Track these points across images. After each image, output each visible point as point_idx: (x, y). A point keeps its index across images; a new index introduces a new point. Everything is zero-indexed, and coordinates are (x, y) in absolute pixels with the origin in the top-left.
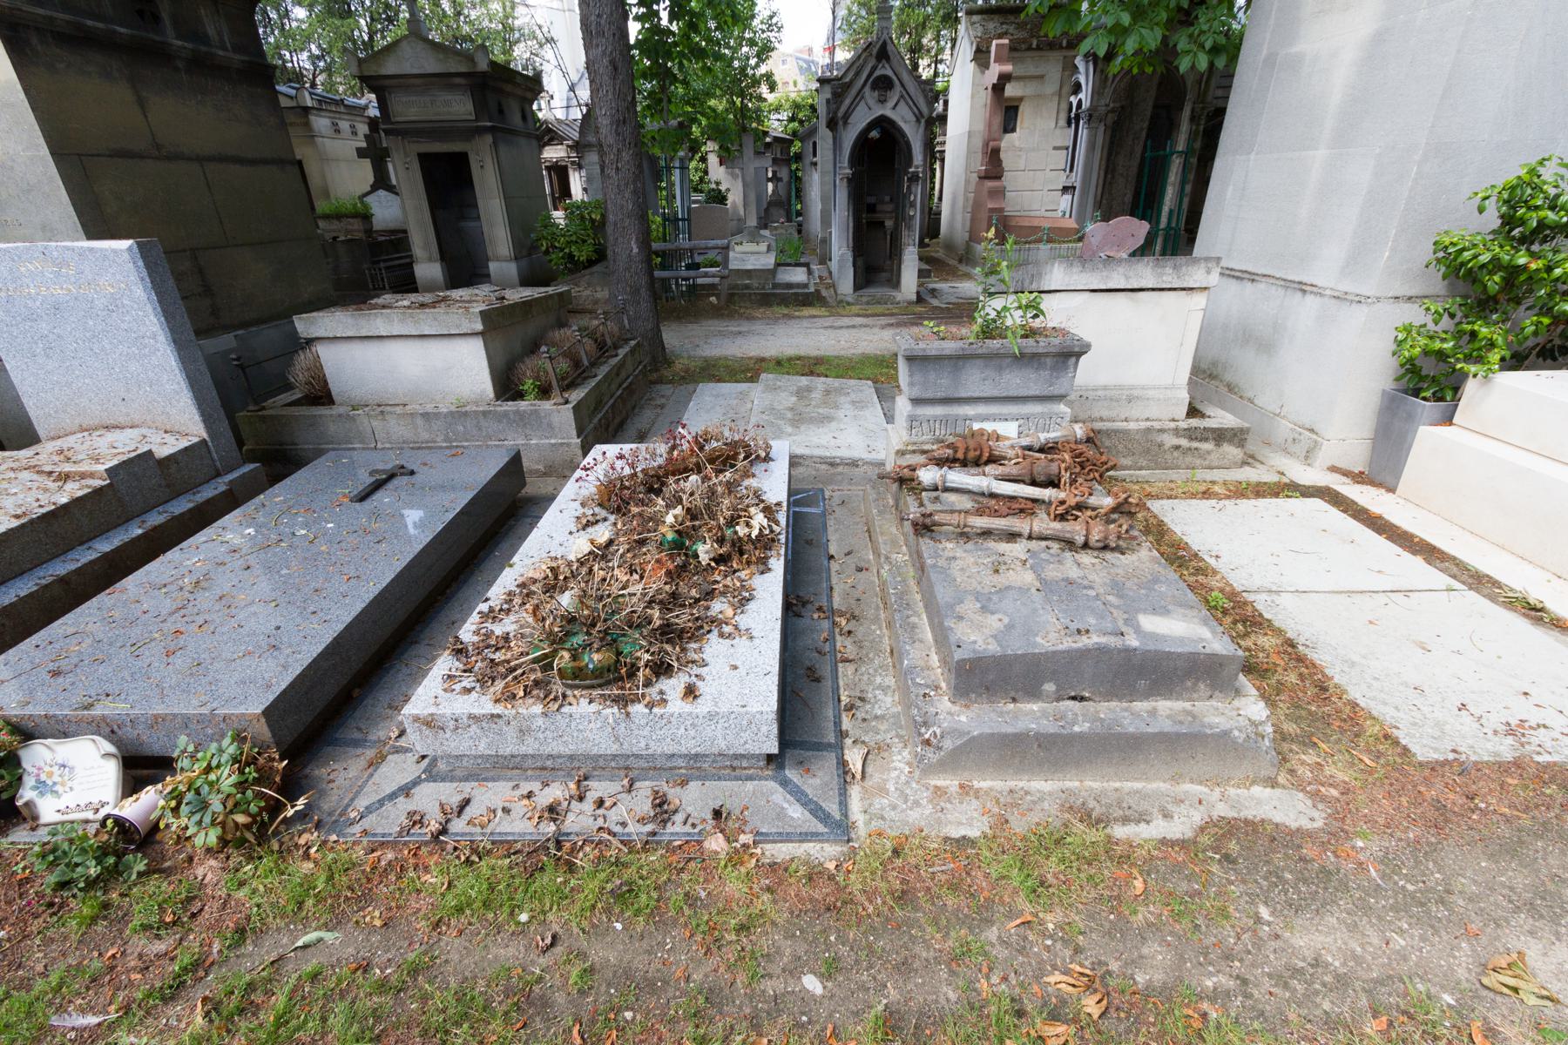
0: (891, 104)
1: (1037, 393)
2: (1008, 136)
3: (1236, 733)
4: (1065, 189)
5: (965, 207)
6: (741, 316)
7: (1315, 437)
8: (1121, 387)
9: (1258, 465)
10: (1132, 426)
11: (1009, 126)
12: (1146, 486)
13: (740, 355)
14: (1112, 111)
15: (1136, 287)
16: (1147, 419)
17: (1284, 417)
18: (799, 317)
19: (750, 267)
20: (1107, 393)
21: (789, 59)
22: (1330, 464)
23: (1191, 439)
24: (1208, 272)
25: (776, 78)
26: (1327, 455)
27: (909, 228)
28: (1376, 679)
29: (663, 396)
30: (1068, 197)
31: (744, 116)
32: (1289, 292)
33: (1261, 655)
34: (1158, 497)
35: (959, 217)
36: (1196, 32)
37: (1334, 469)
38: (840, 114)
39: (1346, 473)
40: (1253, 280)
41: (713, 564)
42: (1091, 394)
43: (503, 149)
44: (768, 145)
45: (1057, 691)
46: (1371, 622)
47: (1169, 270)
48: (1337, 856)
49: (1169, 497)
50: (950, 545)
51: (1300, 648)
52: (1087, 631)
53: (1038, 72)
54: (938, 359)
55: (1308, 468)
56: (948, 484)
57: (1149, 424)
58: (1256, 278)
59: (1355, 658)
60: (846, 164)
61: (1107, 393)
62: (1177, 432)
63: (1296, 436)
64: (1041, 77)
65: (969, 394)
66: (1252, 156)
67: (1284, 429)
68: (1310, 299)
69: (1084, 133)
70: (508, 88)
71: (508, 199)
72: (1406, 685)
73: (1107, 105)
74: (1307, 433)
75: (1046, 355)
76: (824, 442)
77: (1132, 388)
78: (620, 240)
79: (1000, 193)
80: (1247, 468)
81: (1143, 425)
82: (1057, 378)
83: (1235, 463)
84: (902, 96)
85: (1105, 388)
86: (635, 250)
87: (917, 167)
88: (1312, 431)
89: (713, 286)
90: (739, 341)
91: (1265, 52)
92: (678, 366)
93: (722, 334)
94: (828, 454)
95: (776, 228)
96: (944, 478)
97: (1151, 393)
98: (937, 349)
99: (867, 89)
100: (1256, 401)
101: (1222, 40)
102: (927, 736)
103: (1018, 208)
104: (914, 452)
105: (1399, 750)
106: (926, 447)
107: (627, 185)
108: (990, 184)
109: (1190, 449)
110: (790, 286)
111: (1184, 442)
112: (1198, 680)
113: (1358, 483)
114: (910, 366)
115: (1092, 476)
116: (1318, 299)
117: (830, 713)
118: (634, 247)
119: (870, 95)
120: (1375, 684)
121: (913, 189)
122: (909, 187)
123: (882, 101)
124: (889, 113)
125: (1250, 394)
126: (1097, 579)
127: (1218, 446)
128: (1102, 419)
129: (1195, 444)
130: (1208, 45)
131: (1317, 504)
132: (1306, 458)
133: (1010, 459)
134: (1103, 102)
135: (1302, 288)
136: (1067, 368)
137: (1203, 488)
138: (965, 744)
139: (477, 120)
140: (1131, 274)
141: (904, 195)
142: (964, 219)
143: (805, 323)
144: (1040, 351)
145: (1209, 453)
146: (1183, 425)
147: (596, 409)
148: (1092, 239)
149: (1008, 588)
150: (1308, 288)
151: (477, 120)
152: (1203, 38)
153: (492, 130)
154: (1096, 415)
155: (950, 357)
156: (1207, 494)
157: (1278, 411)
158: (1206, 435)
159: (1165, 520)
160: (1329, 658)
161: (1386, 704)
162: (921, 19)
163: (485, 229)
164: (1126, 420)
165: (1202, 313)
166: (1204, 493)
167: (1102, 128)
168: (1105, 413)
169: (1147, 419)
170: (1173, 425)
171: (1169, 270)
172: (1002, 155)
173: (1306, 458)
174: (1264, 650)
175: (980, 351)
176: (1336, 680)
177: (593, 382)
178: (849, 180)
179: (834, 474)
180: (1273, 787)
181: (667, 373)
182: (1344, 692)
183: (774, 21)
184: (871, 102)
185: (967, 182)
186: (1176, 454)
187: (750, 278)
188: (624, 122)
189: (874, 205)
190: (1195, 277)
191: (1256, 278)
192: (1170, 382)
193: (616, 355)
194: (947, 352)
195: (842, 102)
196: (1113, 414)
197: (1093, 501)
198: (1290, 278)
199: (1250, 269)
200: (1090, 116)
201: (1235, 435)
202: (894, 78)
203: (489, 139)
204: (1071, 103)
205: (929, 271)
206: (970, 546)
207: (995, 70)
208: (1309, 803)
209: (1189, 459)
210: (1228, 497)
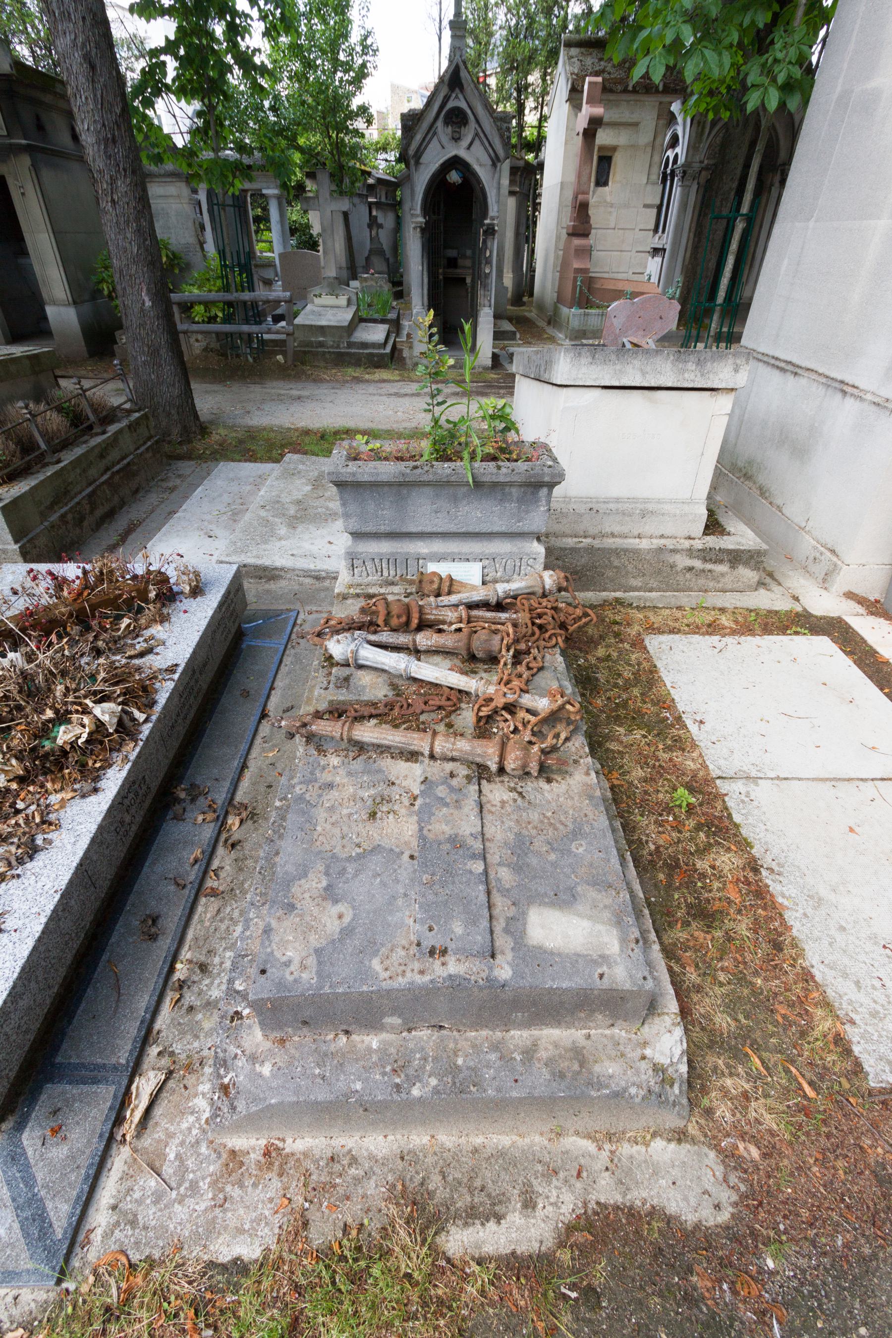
0: (465, 143)
1: (503, 529)
2: (601, 189)
3: (633, 1090)
4: (656, 251)
5: (555, 266)
6: (308, 377)
7: (835, 559)
8: (635, 500)
9: (775, 588)
10: (644, 544)
11: (602, 180)
12: (650, 614)
13: (288, 425)
14: (706, 168)
15: (653, 384)
16: (662, 536)
17: (808, 532)
18: (367, 381)
19: (323, 323)
20: (620, 506)
21: (414, 96)
22: (846, 589)
23: (705, 560)
24: (736, 370)
25: (373, 111)
26: (845, 580)
27: (485, 286)
28: (842, 929)
29: (179, 476)
30: (658, 259)
31: (340, 153)
32: (830, 391)
33: (716, 885)
34: (660, 631)
35: (550, 276)
36: (770, 61)
37: (850, 595)
38: (411, 151)
39: (861, 601)
40: (796, 374)
41: (14, 786)
42: (602, 507)
43: (47, 174)
44: (371, 187)
45: (404, 1023)
46: (851, 830)
47: (691, 366)
48: (735, 1293)
49: (672, 631)
50: (334, 760)
51: (764, 873)
52: (444, 952)
53: (634, 118)
54: (375, 486)
55: (823, 592)
56: (361, 662)
57: (663, 541)
58: (799, 371)
59: (824, 892)
60: (418, 211)
61: (620, 506)
62: (690, 552)
63: (818, 555)
64: (636, 124)
65: (419, 529)
66: (811, 224)
67: (806, 545)
68: (849, 402)
69: (677, 191)
70: (48, 98)
71: (58, 234)
72: (873, 938)
73: (701, 162)
74: (828, 554)
75: (511, 484)
76: (314, 549)
77: (646, 501)
78: (129, 290)
79: (586, 252)
80: (762, 591)
81: (657, 543)
82: (527, 512)
83: (750, 587)
84: (477, 135)
85: (617, 500)
86: (148, 304)
87: (493, 219)
88: (833, 551)
89: (283, 343)
90: (296, 408)
91: (839, 89)
92: (218, 435)
93: (280, 399)
94: (312, 567)
95: (366, 279)
96: (355, 653)
97: (667, 507)
98: (371, 474)
99: (440, 124)
100: (784, 511)
101: (797, 72)
102: (226, 1080)
103: (607, 269)
104: (358, 595)
105: (849, 1066)
106: (371, 591)
107: (127, 222)
108: (577, 242)
109: (703, 571)
110: (365, 345)
111: (698, 564)
112: (593, 1011)
113: (872, 613)
114: (341, 493)
115: (554, 641)
116: (858, 404)
117: (143, 1002)
118: (146, 299)
119: (443, 131)
120: (839, 937)
121: (489, 244)
122: (485, 241)
123: (456, 139)
124: (463, 153)
125: (779, 502)
126: (499, 837)
127: (733, 567)
128: (613, 535)
129: (709, 566)
130: (781, 79)
131: (824, 644)
132: (824, 580)
133: (451, 624)
134: (697, 159)
135: (844, 388)
136: (537, 501)
137: (709, 618)
138: (262, 1110)
139: (9, 136)
140: (648, 368)
141: (481, 250)
142: (553, 279)
143: (372, 389)
144: (502, 479)
145: (723, 575)
146: (698, 544)
147: (56, 502)
148: (615, 321)
149: (377, 849)
150: (849, 390)
151: (9, 136)
152: (776, 69)
153: (28, 149)
154: (608, 530)
155: (389, 484)
156: (712, 628)
157: (803, 525)
158: (721, 556)
159: (659, 664)
160: (791, 891)
161: (845, 976)
162: (527, 53)
163: (37, 268)
164: (639, 537)
165: (726, 418)
166: (709, 625)
167: (695, 187)
168: (617, 529)
169: (662, 536)
170: (687, 544)
171: (691, 366)
172: (591, 212)
173: (824, 580)
174: (720, 877)
175: (425, 478)
176: (794, 932)
177: (50, 471)
178: (423, 231)
179: (319, 590)
180: (679, 1141)
181: (199, 446)
182: (801, 954)
183: (369, 42)
184: (445, 139)
185: (558, 238)
186: (688, 576)
187: (324, 335)
188: (114, 141)
189: (455, 259)
190: (721, 376)
191: (799, 371)
192: (688, 496)
193: (104, 432)
194: (384, 478)
195: (412, 138)
196: (625, 529)
197: (527, 700)
198: (833, 375)
199: (795, 360)
200: (684, 172)
201: (752, 557)
202: (469, 112)
203: (26, 161)
204: (668, 158)
205: (514, 333)
206: (358, 765)
207: (587, 111)
208: (719, 1170)
209: (702, 581)
210: (733, 632)
